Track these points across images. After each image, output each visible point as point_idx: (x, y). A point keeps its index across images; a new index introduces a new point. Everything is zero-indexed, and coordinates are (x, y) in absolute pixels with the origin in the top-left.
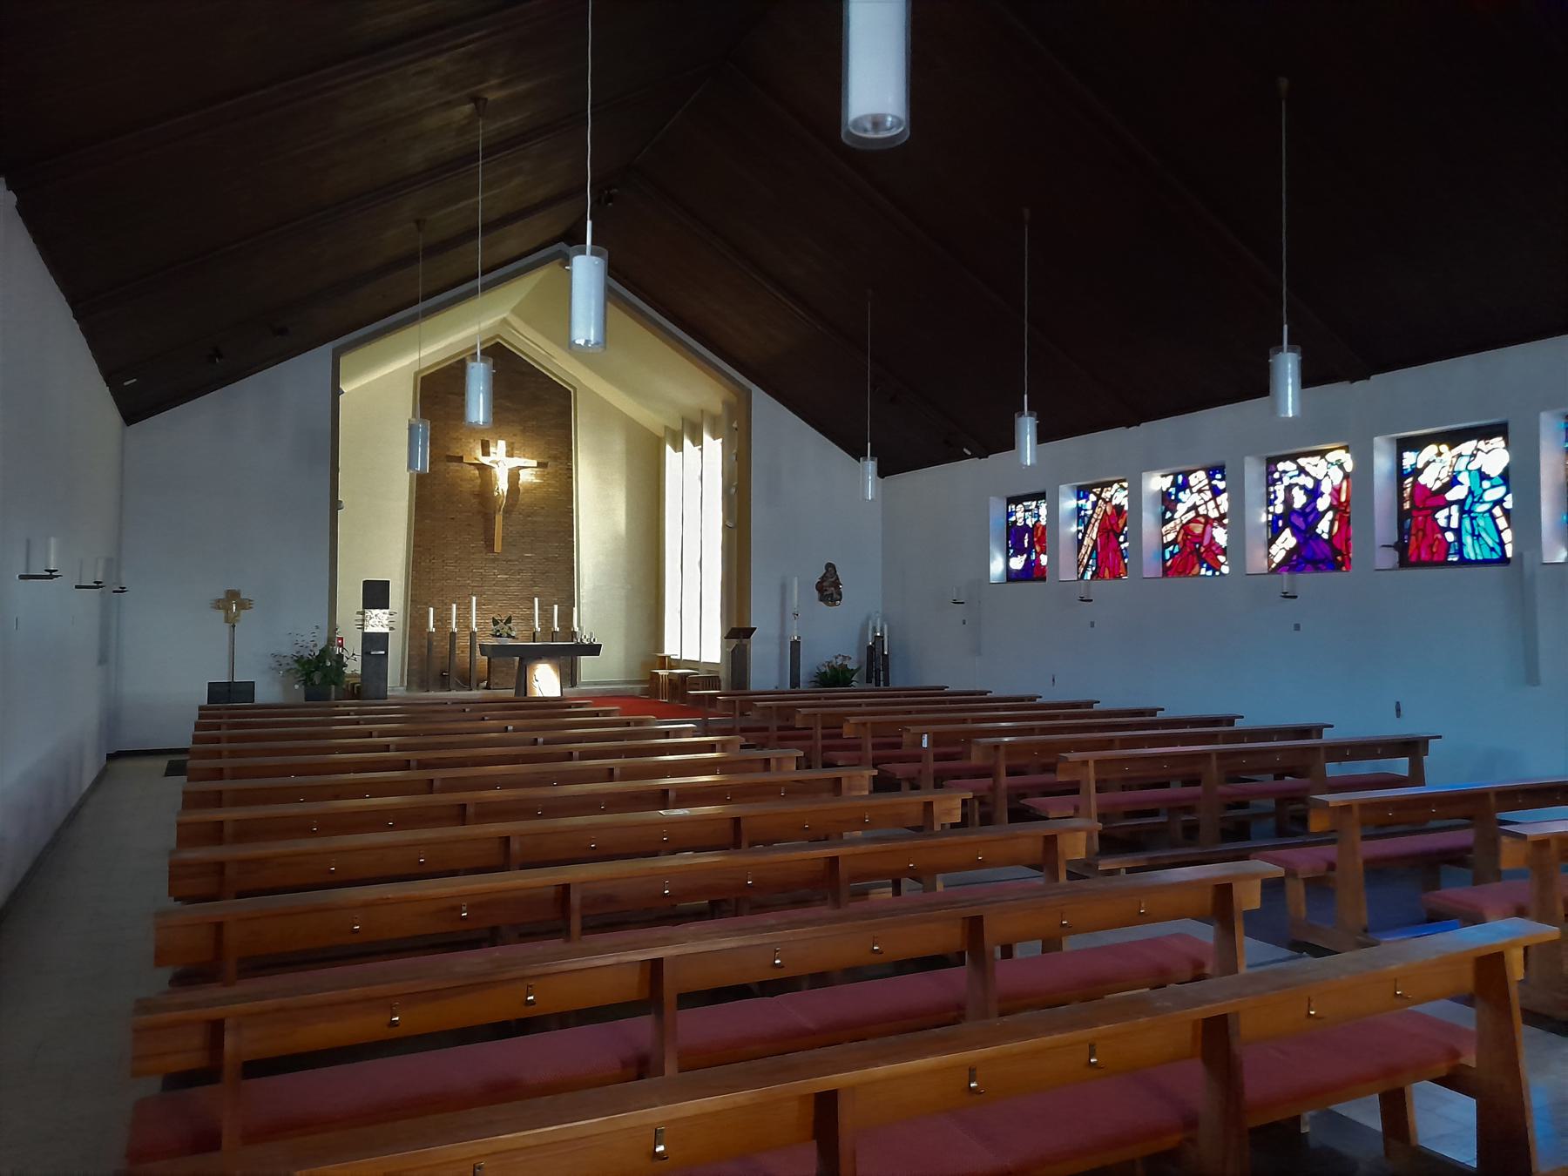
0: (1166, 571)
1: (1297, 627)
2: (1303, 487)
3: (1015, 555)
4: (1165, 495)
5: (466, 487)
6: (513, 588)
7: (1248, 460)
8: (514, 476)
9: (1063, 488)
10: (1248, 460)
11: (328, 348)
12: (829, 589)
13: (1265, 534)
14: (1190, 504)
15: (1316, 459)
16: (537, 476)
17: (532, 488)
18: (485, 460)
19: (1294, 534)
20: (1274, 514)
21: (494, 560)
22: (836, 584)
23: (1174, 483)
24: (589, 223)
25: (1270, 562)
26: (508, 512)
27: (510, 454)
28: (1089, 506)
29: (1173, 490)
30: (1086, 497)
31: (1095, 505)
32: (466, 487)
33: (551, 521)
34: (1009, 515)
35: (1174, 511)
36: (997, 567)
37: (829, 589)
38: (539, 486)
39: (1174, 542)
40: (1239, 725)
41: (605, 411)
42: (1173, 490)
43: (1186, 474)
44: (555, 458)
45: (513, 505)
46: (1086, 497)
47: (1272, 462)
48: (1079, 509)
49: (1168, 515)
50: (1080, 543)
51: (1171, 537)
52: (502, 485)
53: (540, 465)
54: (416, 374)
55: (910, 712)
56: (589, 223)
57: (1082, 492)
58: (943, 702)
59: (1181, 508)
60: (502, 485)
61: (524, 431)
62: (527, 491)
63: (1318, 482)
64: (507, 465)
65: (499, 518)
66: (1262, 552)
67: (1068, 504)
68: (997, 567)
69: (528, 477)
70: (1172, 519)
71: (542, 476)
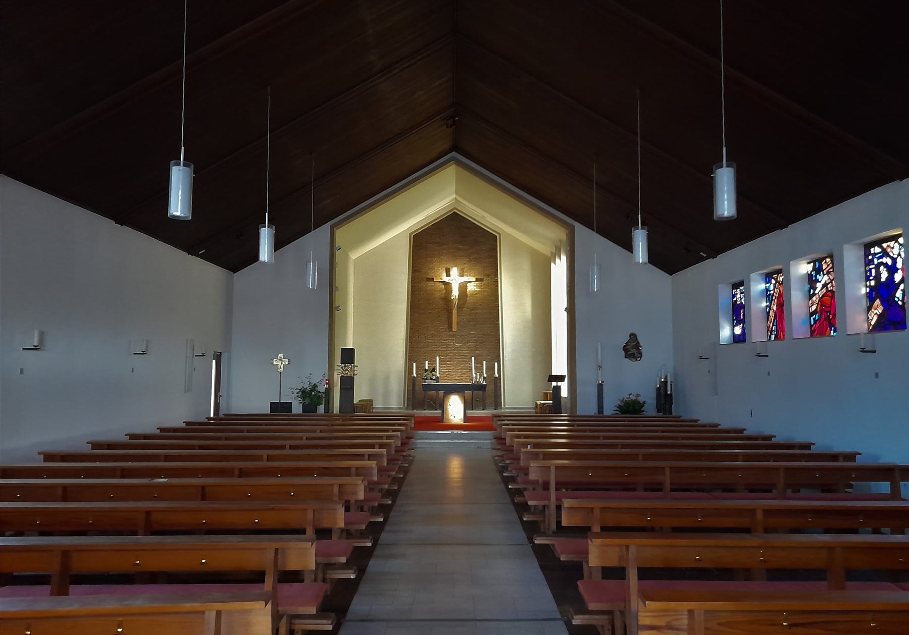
0: (812, 333)
1: (877, 375)
2: (886, 265)
3: (736, 325)
4: (810, 276)
5: (438, 294)
6: (465, 351)
7: (846, 247)
8: (463, 287)
9: (754, 276)
10: (846, 247)
11: (328, 224)
12: (632, 350)
13: (864, 303)
14: (823, 282)
15: (892, 244)
16: (477, 286)
17: (474, 294)
18: (446, 279)
19: (882, 304)
20: (870, 287)
21: (453, 336)
22: (637, 346)
23: (814, 269)
24: (724, 149)
25: (869, 324)
26: (460, 307)
27: (462, 275)
28: (772, 287)
29: (813, 273)
30: (770, 282)
31: (775, 285)
32: (438, 294)
33: (485, 313)
34: (734, 296)
35: (815, 289)
36: (725, 333)
37: (632, 350)
38: (478, 292)
39: (815, 312)
40: (814, 449)
41: (517, 246)
42: (813, 273)
43: (820, 260)
44: (488, 275)
45: (464, 304)
46: (770, 282)
47: (868, 246)
48: (767, 290)
49: (812, 292)
50: (768, 313)
51: (814, 308)
52: (455, 293)
53: (477, 280)
54: (411, 234)
55: (585, 431)
56: (724, 149)
57: (768, 277)
58: (638, 426)
59: (819, 286)
60: (455, 293)
61: (470, 261)
62: (472, 295)
63: (894, 260)
64: (457, 279)
65: (455, 312)
66: (862, 317)
67: (759, 287)
68: (725, 333)
69: (472, 287)
70: (814, 294)
71: (480, 287)
